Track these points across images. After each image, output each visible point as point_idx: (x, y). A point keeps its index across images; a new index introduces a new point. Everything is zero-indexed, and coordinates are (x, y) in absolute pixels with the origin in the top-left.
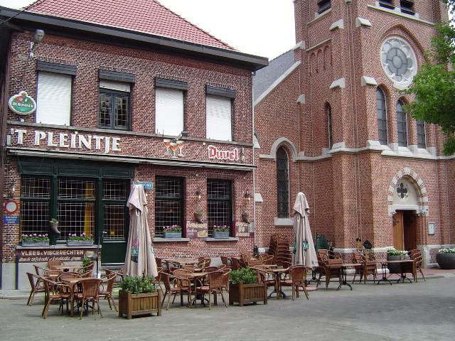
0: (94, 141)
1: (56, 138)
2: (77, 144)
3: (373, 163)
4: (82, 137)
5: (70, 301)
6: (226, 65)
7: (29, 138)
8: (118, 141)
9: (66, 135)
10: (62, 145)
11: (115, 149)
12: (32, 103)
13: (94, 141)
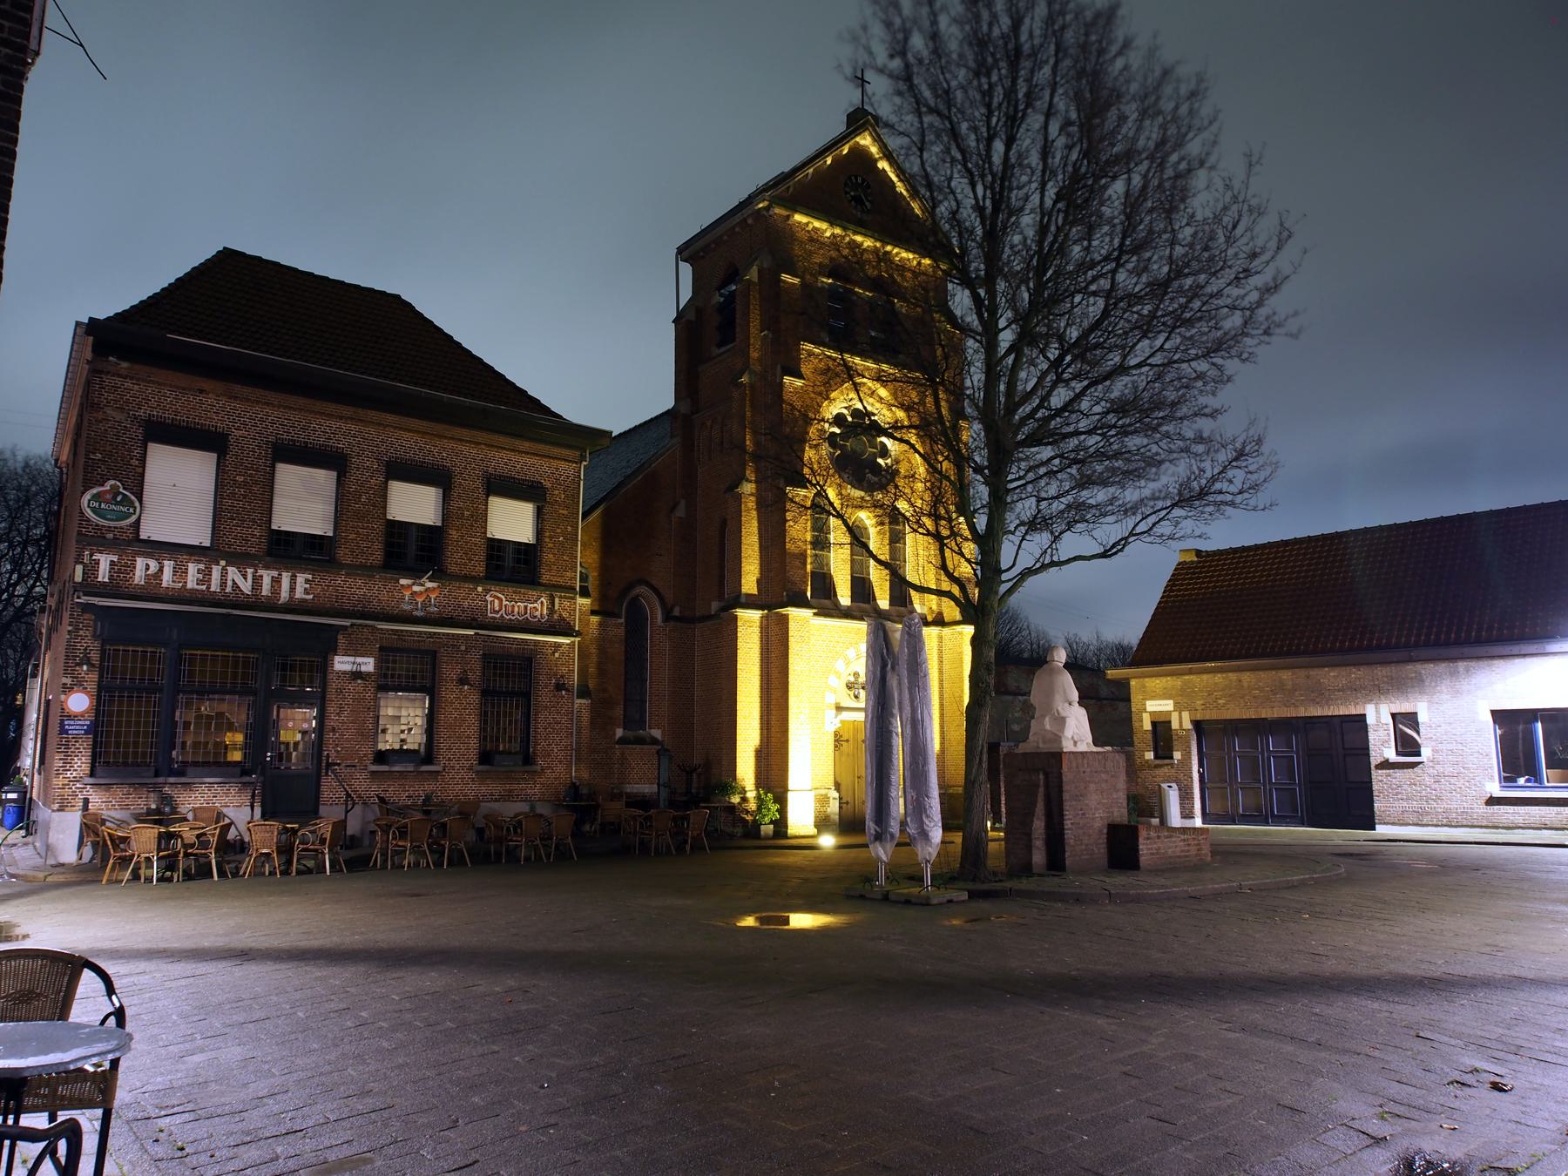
0: (257, 581)
1: (180, 572)
2: (223, 584)
3: (81, 990)
4: (233, 573)
5: (78, 324)
6: (1038, 754)
7: (122, 570)
8: (307, 581)
9: (202, 566)
11: (299, 594)
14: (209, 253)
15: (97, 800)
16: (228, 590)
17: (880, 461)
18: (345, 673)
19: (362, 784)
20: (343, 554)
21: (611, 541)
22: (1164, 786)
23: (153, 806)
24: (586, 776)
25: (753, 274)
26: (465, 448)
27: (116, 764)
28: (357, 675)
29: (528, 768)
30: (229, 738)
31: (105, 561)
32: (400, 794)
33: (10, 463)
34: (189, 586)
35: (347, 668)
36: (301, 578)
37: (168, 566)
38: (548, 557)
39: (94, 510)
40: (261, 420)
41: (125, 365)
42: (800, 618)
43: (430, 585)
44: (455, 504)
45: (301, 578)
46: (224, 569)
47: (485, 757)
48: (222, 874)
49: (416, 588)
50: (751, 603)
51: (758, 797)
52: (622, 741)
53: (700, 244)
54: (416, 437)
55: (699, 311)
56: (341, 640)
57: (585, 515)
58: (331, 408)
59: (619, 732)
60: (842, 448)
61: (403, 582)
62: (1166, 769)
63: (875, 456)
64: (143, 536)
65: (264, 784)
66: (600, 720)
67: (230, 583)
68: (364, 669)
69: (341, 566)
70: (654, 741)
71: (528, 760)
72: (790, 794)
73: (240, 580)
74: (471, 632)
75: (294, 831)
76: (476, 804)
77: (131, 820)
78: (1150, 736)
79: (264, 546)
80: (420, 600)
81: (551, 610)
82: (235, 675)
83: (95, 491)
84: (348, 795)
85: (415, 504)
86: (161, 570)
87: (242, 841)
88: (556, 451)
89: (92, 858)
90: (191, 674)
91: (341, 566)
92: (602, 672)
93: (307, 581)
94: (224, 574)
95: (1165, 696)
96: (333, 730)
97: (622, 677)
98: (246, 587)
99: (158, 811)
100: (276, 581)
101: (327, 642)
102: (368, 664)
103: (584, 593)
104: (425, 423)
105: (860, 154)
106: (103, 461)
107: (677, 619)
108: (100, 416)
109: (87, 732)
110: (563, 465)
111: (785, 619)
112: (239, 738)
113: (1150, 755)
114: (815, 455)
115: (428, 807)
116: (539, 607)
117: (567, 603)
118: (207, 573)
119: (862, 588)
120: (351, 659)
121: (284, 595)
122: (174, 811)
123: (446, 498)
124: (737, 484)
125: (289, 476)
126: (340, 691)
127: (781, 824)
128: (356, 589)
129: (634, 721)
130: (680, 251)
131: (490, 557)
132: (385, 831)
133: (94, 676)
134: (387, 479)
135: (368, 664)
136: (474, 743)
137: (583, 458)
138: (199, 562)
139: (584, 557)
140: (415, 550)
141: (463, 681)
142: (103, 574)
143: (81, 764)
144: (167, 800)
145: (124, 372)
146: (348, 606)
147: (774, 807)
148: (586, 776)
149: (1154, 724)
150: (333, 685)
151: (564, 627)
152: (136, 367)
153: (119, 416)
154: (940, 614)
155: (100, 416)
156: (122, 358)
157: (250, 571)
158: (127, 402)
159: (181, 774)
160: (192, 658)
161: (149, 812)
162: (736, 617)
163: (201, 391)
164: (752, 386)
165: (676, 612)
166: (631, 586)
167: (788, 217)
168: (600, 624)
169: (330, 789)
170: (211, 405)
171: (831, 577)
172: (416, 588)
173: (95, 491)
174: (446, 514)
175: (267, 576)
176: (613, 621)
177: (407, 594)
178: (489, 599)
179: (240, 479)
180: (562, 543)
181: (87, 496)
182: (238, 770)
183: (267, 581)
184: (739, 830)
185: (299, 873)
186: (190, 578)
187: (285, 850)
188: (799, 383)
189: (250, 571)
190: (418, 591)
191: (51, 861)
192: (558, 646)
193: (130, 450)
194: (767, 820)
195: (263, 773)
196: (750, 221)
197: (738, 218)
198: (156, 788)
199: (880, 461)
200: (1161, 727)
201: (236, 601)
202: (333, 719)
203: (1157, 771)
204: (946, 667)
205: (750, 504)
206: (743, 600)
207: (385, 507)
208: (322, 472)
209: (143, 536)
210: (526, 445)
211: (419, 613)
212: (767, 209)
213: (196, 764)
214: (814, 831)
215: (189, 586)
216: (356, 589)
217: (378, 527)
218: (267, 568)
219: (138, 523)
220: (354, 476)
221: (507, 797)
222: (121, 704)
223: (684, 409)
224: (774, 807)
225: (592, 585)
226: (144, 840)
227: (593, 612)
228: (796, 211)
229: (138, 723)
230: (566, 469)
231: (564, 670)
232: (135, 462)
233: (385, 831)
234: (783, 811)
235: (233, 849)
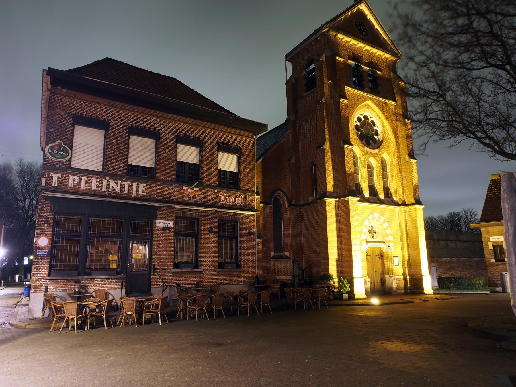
0: (122, 187)
2: (108, 188)
4: (112, 183)
5: (44, 70)
7: (63, 181)
10: (94, 188)
11: (141, 193)
12: (67, 151)
13: (122, 187)
14: (102, 58)
15: (52, 287)
16: (110, 190)
17: (375, 137)
18: (160, 228)
19: (169, 278)
20: (159, 175)
21: (266, 172)
22: (504, 273)
23: (77, 290)
24: (261, 272)
25: (323, 58)
26: (208, 131)
27: (60, 270)
28: (166, 229)
29: (238, 270)
30: (111, 258)
31: (55, 177)
32: (185, 282)
33: (36, 167)
34: (93, 188)
35: (162, 225)
36: (141, 186)
37: (84, 179)
38: (243, 178)
39: (50, 153)
40: (124, 116)
41: (65, 90)
42: (353, 200)
43: (195, 189)
44: (205, 155)
45: (141, 186)
46: (108, 181)
47: (220, 265)
48: (109, 325)
49: (190, 191)
50: (331, 196)
51: (340, 281)
52: (274, 257)
53: (294, 53)
54: (188, 126)
55: (296, 79)
56: (159, 213)
57: (257, 160)
58: (153, 112)
59: (273, 254)
60: (361, 131)
61: (184, 188)
62: (502, 266)
63: (373, 135)
64: (73, 166)
65: (126, 278)
66: (266, 249)
67: (111, 187)
68: (169, 226)
69: (158, 181)
70: (287, 257)
71: (238, 266)
72: (355, 280)
73: (115, 186)
74: (213, 210)
75: (143, 302)
76: (218, 286)
77: (68, 298)
78: (492, 252)
79: (125, 171)
80: (191, 196)
81: (245, 201)
82: (113, 229)
83: (51, 145)
84: (164, 283)
85: (188, 154)
86: (80, 181)
87: (117, 305)
89: (49, 315)
90: (94, 228)
91: (158, 181)
92: (265, 228)
93: (144, 187)
94: (108, 184)
95: (499, 234)
96: (156, 253)
97: (273, 229)
98: (118, 189)
99: (79, 292)
100: (131, 187)
101: (152, 214)
102: (171, 224)
103: (258, 194)
104: (191, 120)
105: (361, 13)
106: (55, 132)
107: (293, 205)
108: (54, 112)
109: (47, 255)
110: (248, 139)
111: (347, 202)
112: (115, 257)
113: (493, 260)
114: (353, 134)
115: (198, 288)
116: (240, 199)
117: (251, 198)
118: (101, 183)
119: (373, 190)
120: (163, 222)
121: (134, 193)
122: (86, 292)
123: (201, 152)
124: (323, 144)
125: (135, 141)
126: (159, 236)
127: (351, 293)
128: (165, 190)
129: (278, 248)
130: (286, 56)
131: (219, 178)
132: (185, 301)
133: (51, 229)
134: (177, 143)
135: (171, 224)
136: (215, 259)
138: (97, 178)
139: (257, 180)
140: (189, 174)
141: (210, 231)
142: (55, 183)
143: (44, 270)
144: (83, 287)
145: (64, 94)
146: (161, 198)
147: (348, 286)
148: (261, 272)
149: (494, 246)
150: (156, 233)
151: (249, 208)
152: (70, 92)
153: (62, 113)
154: (404, 201)
155: (54, 112)
156: (63, 87)
157: (119, 182)
158: (66, 106)
159: (90, 274)
160: (95, 221)
161: (75, 293)
162: (325, 202)
163: (98, 103)
164: (326, 104)
165: (293, 202)
166: (275, 192)
167: (336, 35)
168: (263, 207)
169: (155, 280)
170: (101, 109)
171: (360, 185)
172: (190, 191)
173: (51, 145)
174: (201, 159)
175: (127, 184)
176: (268, 206)
177: (186, 193)
178: (220, 195)
179: (115, 142)
180: (248, 172)
181: (48, 147)
182: (115, 272)
184: (332, 296)
185: (146, 323)
186: (93, 185)
187: (139, 312)
188: (346, 101)
189: (119, 182)
190: (191, 191)
191: (31, 317)
192: (248, 216)
193: (67, 128)
194: (345, 291)
195: (126, 273)
196: (319, 38)
197: (314, 38)
198: (78, 281)
199: (375, 137)
200: (498, 248)
201: (113, 195)
202: (156, 249)
203: (497, 267)
204: (408, 223)
205: (328, 155)
206: (328, 194)
207: (176, 155)
208: (150, 140)
209: (73, 166)
210: (232, 130)
211: (191, 202)
212: (327, 32)
213: (96, 270)
214: (365, 296)
215: (93, 188)
216: (165, 190)
217: (173, 164)
218: (127, 181)
219: (70, 160)
220: (163, 141)
221: (230, 283)
222: (63, 243)
223: (293, 118)
224: (348, 286)
225: (260, 190)
226: (71, 309)
227: (261, 203)
228: (339, 33)
229: (70, 251)
230: (249, 141)
231: (251, 226)
232: (69, 133)
233: (185, 301)
234: (352, 287)
235: (113, 308)
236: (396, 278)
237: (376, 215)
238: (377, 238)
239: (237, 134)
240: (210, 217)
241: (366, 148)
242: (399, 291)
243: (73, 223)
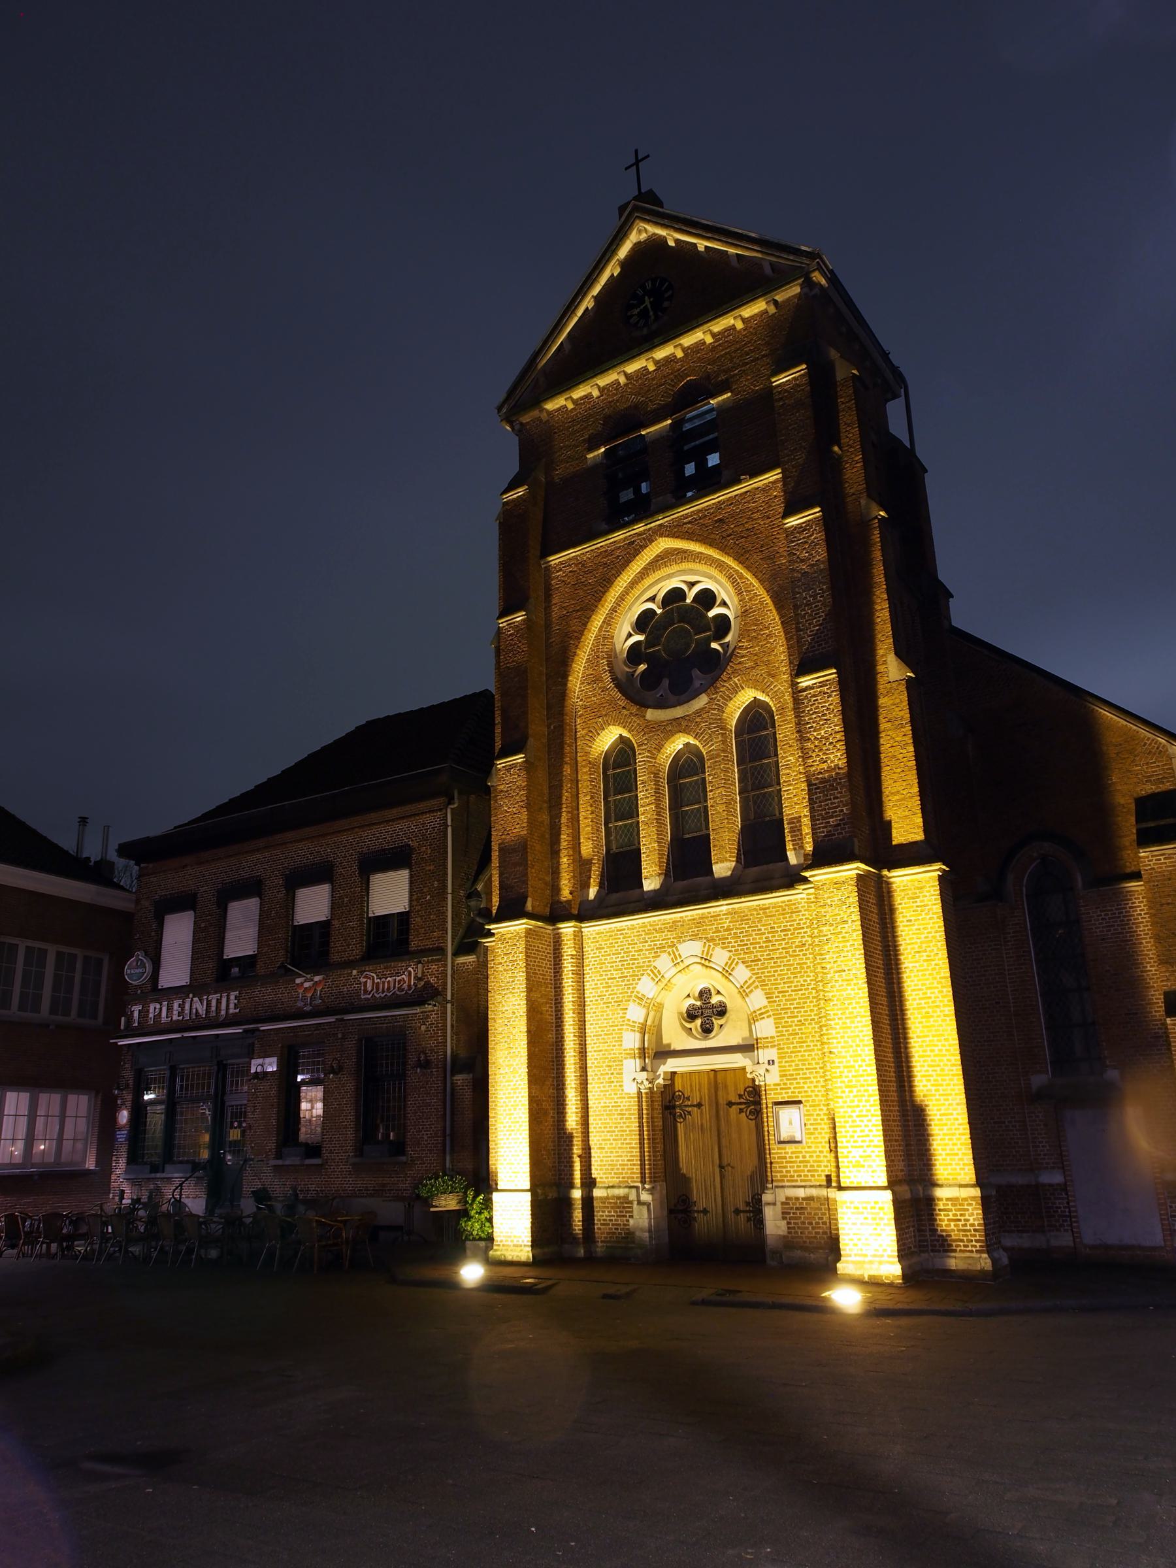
5: (681, 1014)
41: (151, 866)
61: (298, 981)
74: (331, 1019)
85: (313, 905)
88: (423, 806)
98: (202, 1010)
110: (429, 818)
137: (451, 800)
172: (306, 985)
180: (429, 902)
183: (214, 1003)
211: (308, 1008)
230: (431, 821)
236: (782, 1195)
237: (691, 949)
238: (729, 1033)
239: (403, 818)
240: (340, 1036)
241: (651, 714)
242: (799, 1253)
243: (198, 1079)
